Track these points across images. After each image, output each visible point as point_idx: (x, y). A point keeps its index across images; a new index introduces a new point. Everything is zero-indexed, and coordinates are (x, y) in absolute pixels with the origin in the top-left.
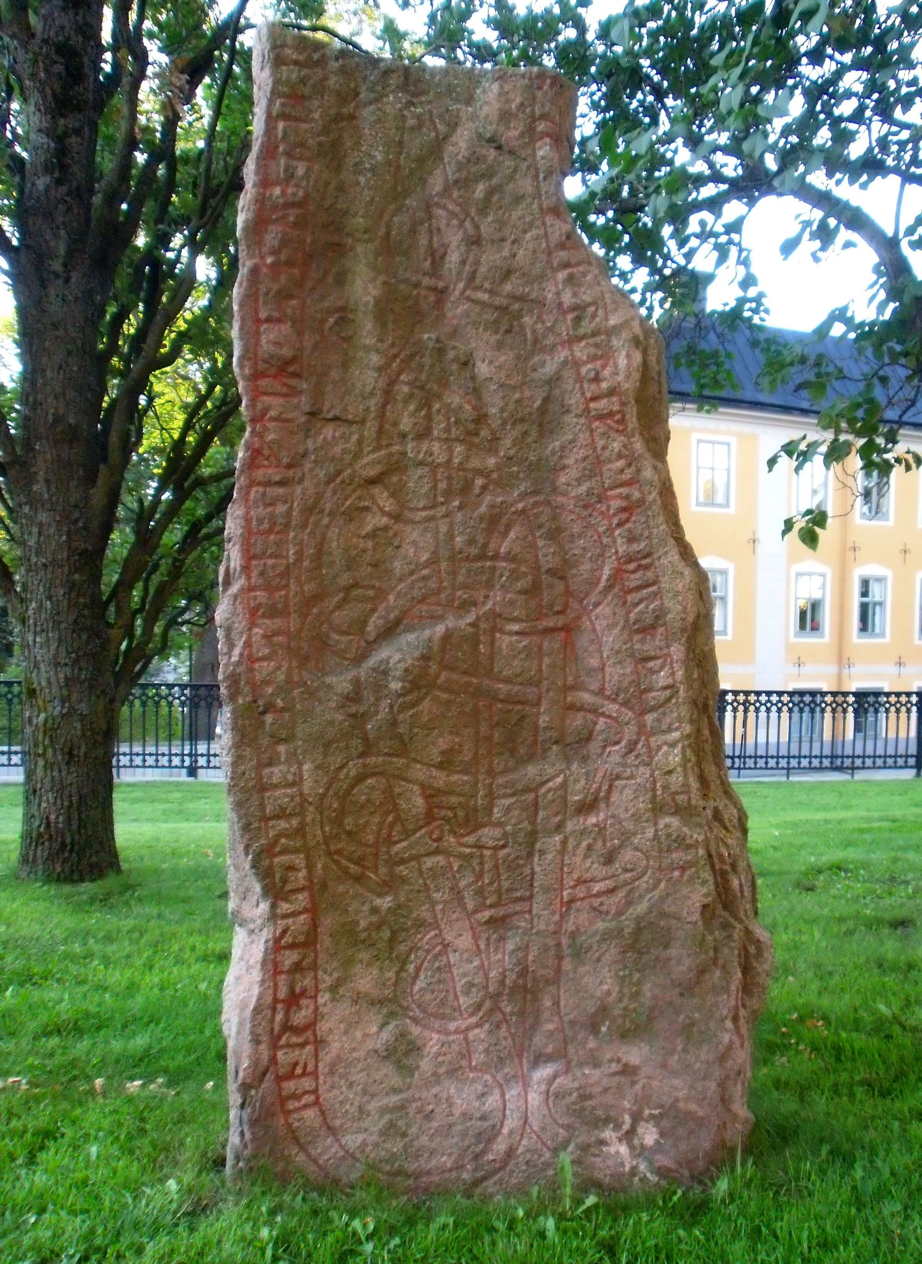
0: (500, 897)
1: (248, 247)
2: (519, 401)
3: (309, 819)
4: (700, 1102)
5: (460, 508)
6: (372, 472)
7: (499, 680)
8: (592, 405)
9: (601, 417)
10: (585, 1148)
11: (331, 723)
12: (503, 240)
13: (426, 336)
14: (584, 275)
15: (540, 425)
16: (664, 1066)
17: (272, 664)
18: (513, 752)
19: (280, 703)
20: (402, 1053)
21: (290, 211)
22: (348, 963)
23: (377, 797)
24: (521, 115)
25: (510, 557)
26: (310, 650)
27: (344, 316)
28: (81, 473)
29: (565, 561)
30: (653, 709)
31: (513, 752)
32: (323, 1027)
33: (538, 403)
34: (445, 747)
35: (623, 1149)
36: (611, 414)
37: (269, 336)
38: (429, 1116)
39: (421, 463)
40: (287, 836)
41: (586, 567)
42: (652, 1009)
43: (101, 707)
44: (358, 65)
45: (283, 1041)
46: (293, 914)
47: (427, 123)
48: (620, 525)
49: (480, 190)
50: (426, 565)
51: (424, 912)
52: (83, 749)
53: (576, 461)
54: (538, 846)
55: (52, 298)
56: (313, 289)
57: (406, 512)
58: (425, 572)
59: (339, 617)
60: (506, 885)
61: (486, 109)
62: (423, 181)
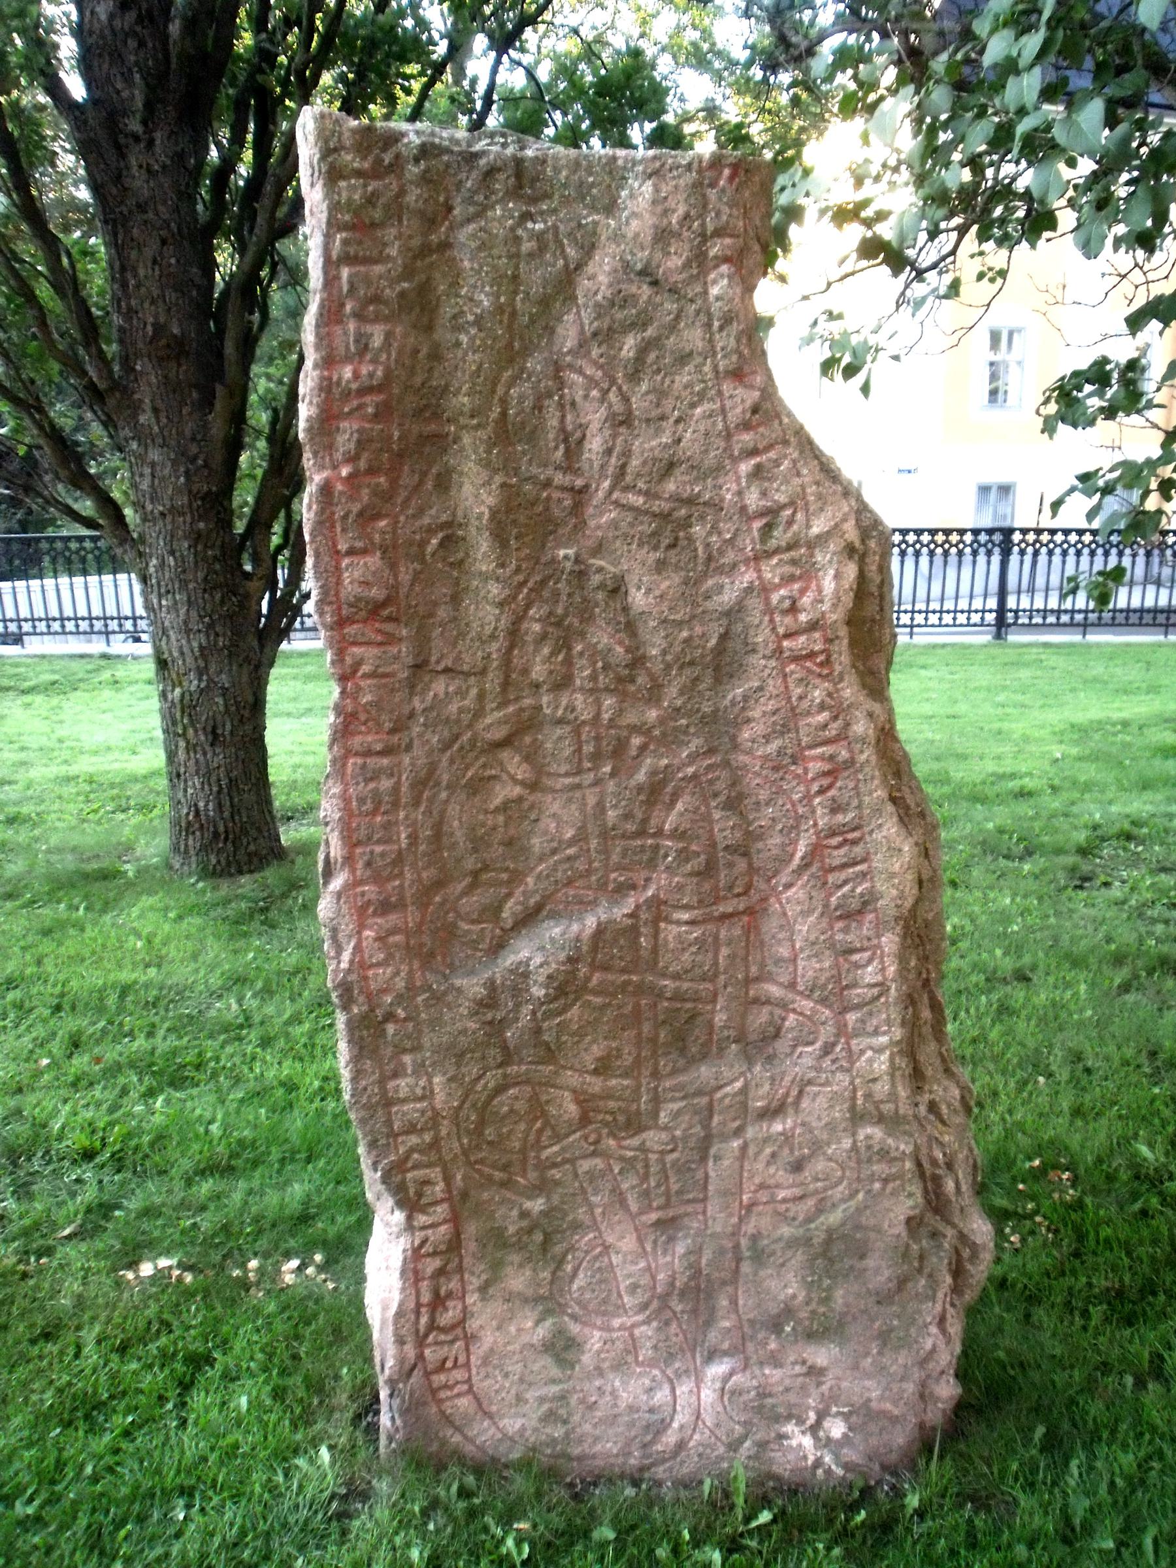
0: (668, 1200)
1: (315, 454)
2: (687, 641)
3: (444, 1132)
4: (895, 1403)
5: (613, 775)
6: (499, 734)
7: (664, 975)
8: (785, 643)
9: (796, 659)
10: (762, 1445)
11: (464, 1032)
12: (662, 418)
13: (562, 553)
14: (777, 463)
15: (717, 669)
16: (856, 1367)
17: (389, 970)
18: (683, 1051)
19: (401, 1013)
20: (562, 1349)
21: (368, 399)
22: (496, 1266)
23: (521, 1106)
24: (686, 234)
25: (677, 834)
26: (434, 947)
27: (452, 537)
28: (195, 395)
29: (748, 833)
30: (858, 1007)
31: (683, 1051)
32: (473, 1325)
33: (713, 642)
34: (599, 1054)
35: (807, 1441)
36: (812, 655)
37: (353, 573)
38: (593, 1406)
39: (560, 722)
40: (420, 1152)
41: (775, 840)
42: (844, 1315)
43: (245, 679)
44: (448, 165)
45: (431, 1338)
46: (433, 1226)
47: (552, 246)
48: (822, 791)
49: (629, 345)
50: (572, 842)
51: (581, 1213)
52: (228, 727)
53: (764, 713)
54: (713, 1151)
55: (135, 170)
56: (406, 503)
57: (545, 780)
58: (571, 851)
59: (472, 903)
60: (675, 1187)
61: (635, 223)
62: (550, 331)
